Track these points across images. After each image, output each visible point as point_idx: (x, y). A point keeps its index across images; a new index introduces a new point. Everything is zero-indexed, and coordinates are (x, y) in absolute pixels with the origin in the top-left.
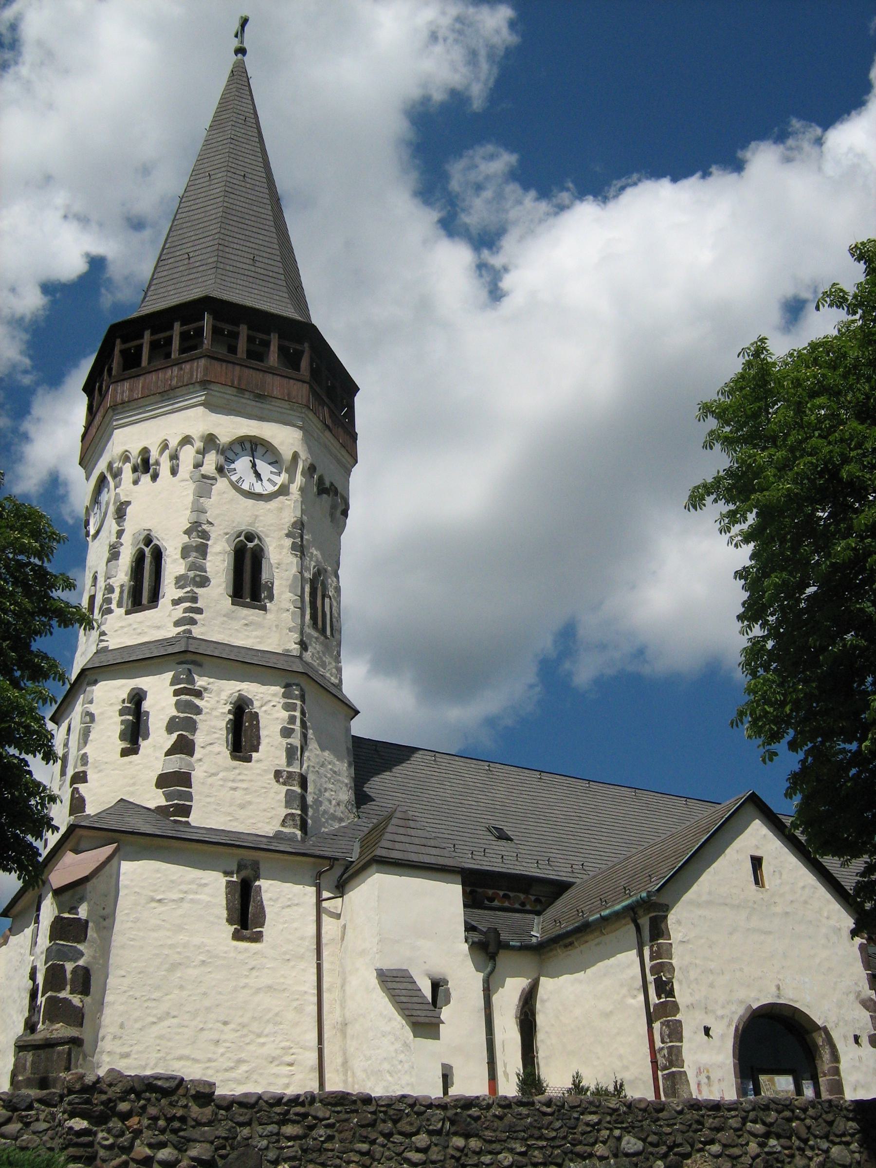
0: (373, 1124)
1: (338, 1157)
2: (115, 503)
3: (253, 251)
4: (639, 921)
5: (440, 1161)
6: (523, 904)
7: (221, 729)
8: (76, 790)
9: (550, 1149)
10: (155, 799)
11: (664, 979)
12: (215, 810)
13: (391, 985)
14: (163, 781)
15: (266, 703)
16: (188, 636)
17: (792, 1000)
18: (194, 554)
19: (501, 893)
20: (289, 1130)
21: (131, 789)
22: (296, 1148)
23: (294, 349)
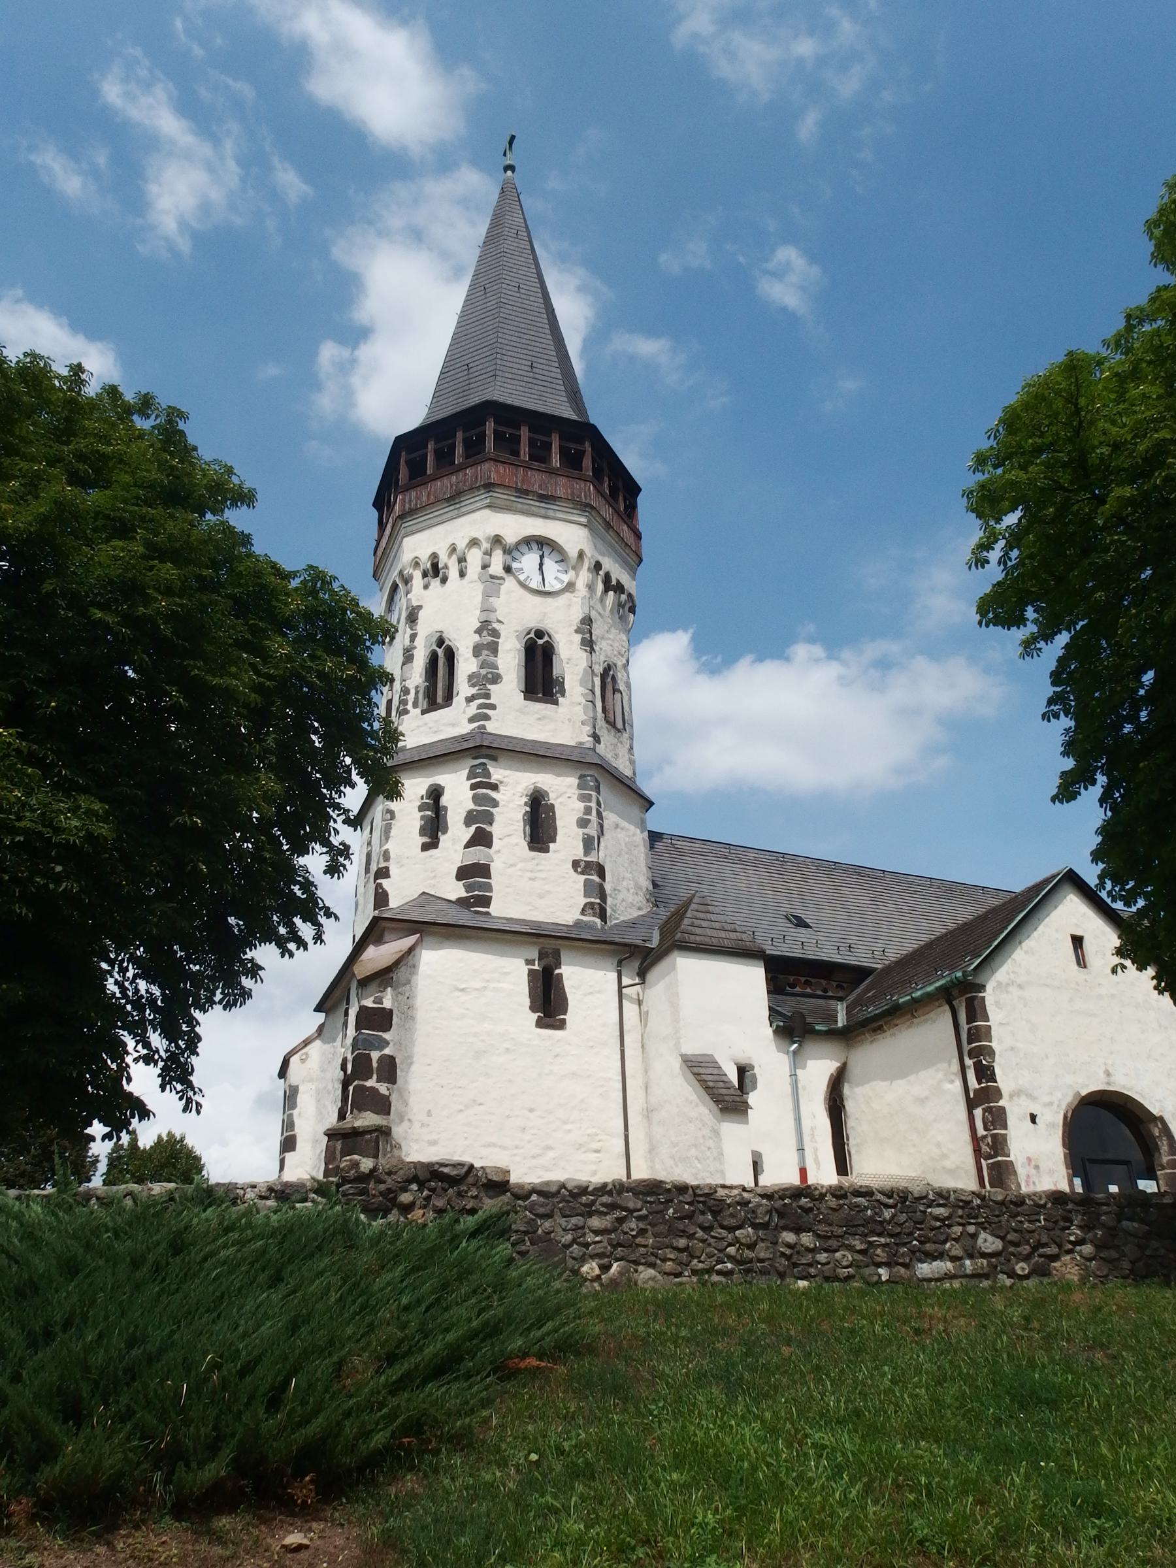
0: (690, 1216)
1: (652, 1254)
2: (407, 608)
3: (530, 358)
4: (954, 1003)
5: (769, 1259)
6: (825, 991)
7: (518, 822)
8: (379, 886)
9: (895, 1248)
10: (456, 891)
11: (984, 1062)
12: (515, 900)
13: (696, 1070)
14: (464, 873)
15: (561, 795)
16: (482, 730)
17: (1124, 1087)
18: (485, 652)
19: (803, 979)
20: (595, 1222)
21: (432, 882)
22: (605, 1243)
23: (575, 450)
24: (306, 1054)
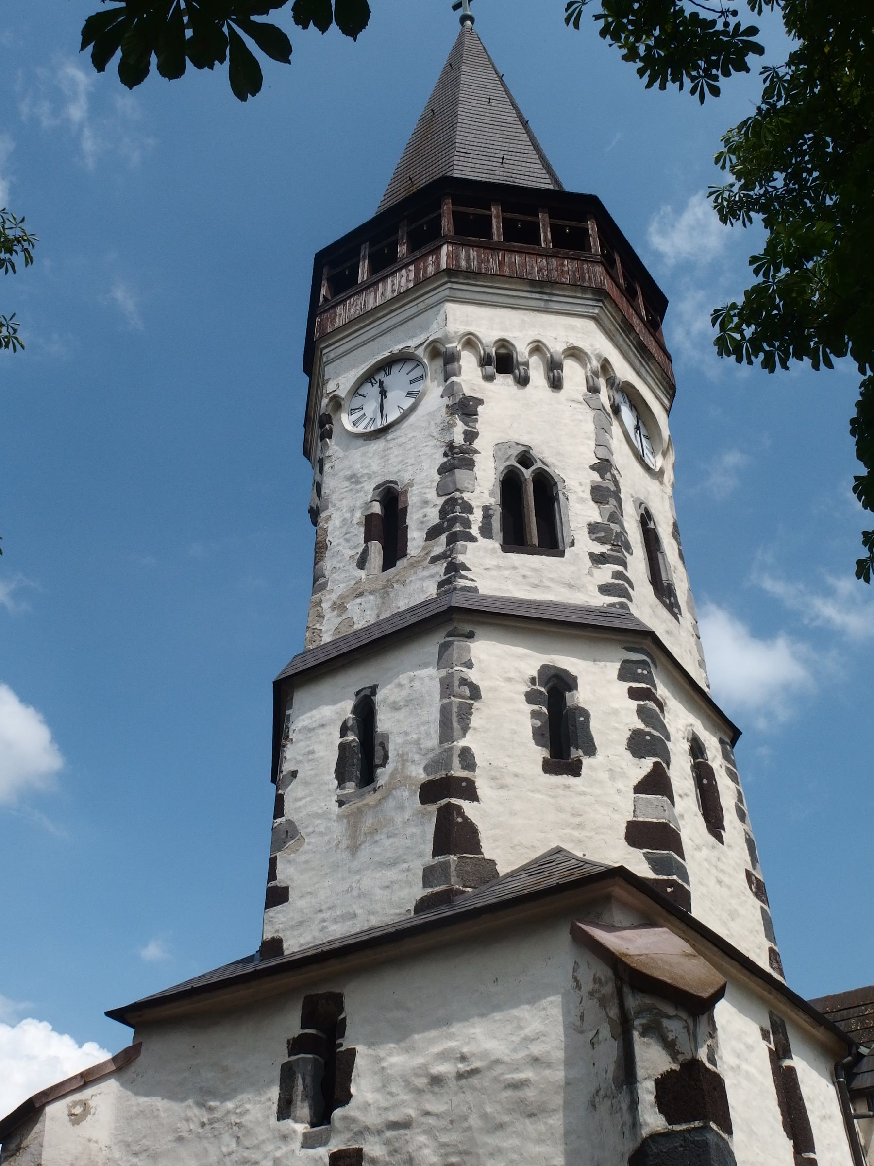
24: (85, 1104)
